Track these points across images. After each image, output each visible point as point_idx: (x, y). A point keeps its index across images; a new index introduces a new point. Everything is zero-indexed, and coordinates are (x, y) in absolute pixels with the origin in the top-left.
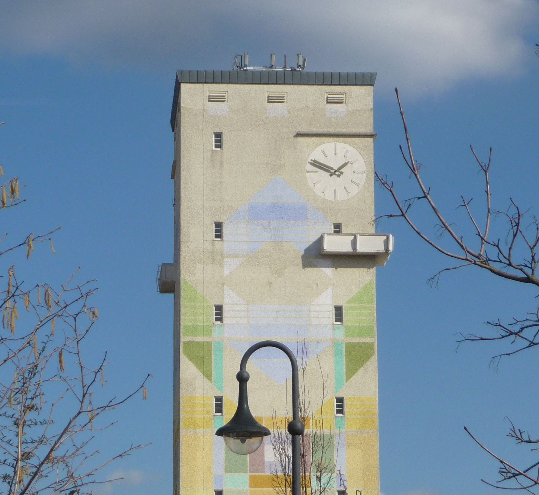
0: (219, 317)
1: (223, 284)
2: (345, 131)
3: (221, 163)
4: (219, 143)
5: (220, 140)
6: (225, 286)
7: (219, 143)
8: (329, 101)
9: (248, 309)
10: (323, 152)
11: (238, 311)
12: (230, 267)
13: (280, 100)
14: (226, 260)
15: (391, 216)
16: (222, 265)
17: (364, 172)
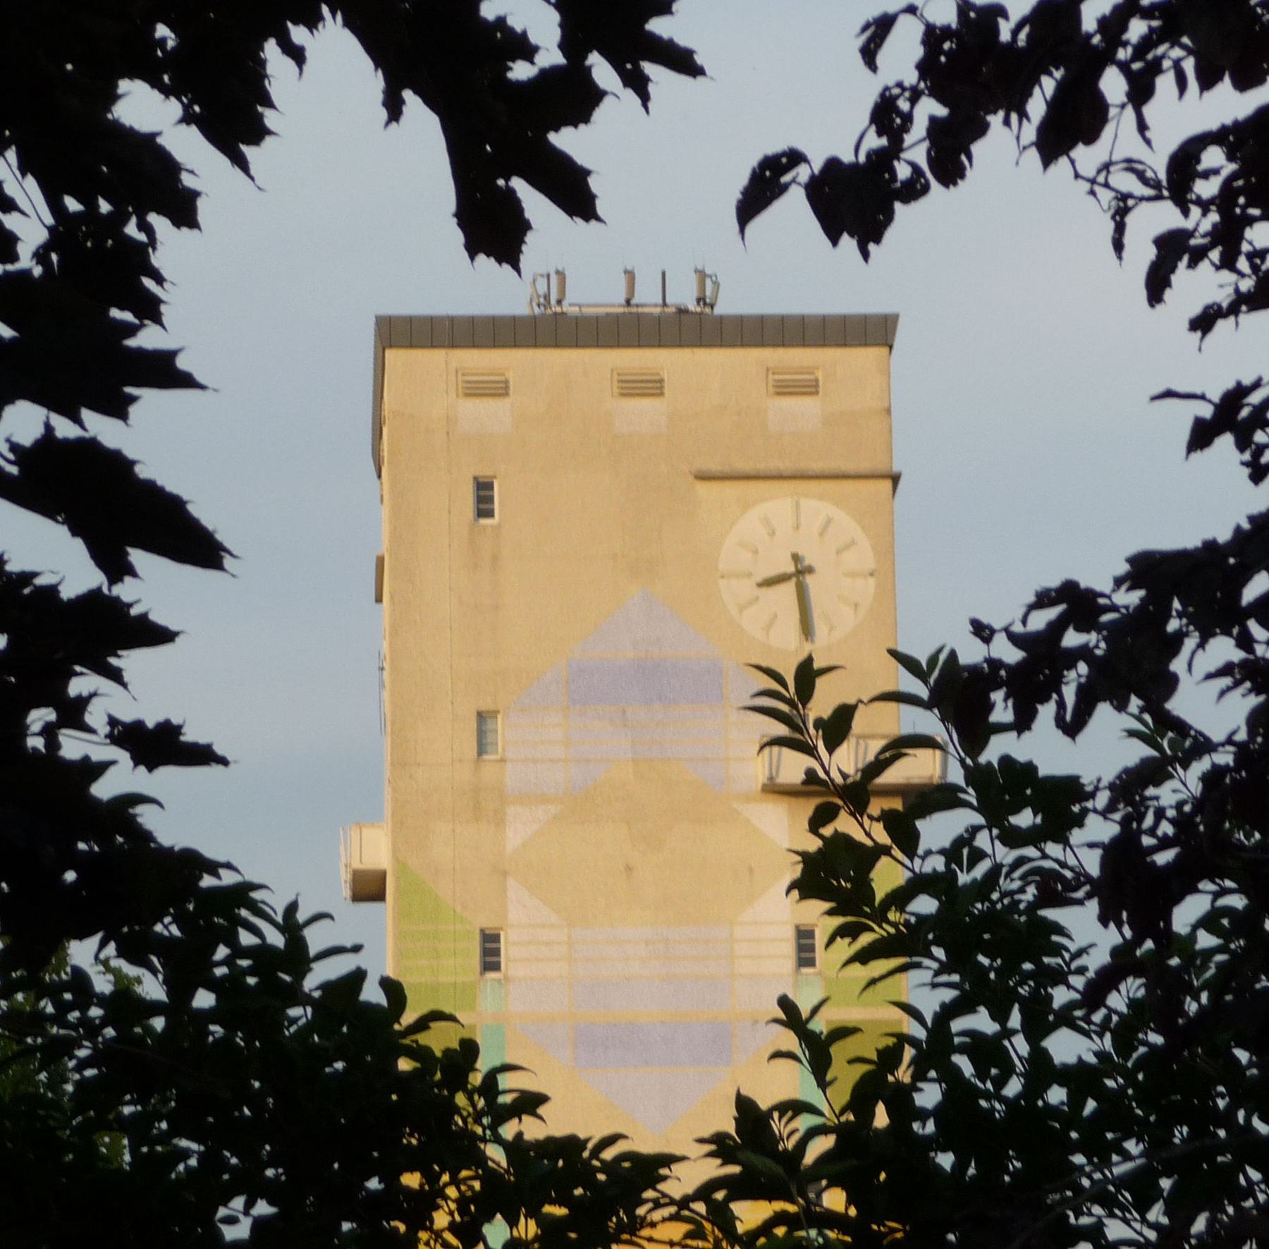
0: (490, 958)
1: (505, 874)
2: (817, 466)
3: (495, 559)
4: (484, 506)
5: (478, 502)
6: (511, 882)
7: (484, 506)
8: (785, 389)
9: (569, 937)
10: (766, 521)
11: (547, 944)
12: (520, 829)
13: (652, 387)
14: (511, 810)
15: (1169, 394)
16: (500, 821)
17: (871, 574)
